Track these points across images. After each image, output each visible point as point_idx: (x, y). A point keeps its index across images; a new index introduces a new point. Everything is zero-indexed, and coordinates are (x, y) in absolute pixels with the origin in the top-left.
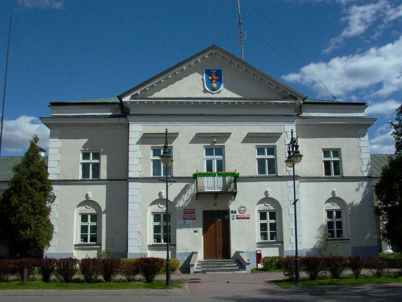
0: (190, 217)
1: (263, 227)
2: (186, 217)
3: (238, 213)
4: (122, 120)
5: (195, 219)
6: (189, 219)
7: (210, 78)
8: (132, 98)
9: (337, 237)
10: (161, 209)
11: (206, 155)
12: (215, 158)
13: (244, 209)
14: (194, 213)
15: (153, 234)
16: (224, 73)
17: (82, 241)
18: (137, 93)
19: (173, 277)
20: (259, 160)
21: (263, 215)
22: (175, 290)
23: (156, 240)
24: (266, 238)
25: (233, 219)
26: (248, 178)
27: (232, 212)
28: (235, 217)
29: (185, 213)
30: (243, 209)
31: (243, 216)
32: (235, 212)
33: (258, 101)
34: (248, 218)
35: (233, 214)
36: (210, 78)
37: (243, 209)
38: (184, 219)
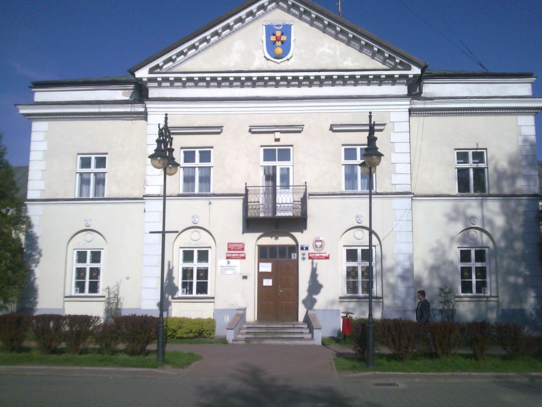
0: (237, 255)
1: (80, 272)
2: (230, 255)
3: (311, 250)
4: (139, 109)
5: (244, 258)
6: (236, 258)
7: (273, 38)
8: (151, 71)
9: (90, 292)
10: (360, 239)
11: (345, 159)
12: (279, 165)
13: (320, 243)
14: (243, 249)
15: (209, 281)
16: (295, 32)
17: (76, 290)
18: (158, 64)
19: (170, 348)
20: (266, 169)
21: (351, 255)
22: (168, 370)
23: (78, 289)
24: (82, 290)
25: (304, 259)
26: (95, 191)
27: (302, 249)
28: (307, 256)
29: (229, 249)
30: (319, 243)
31: (318, 255)
32: (307, 249)
33: (312, 75)
34: (327, 258)
35: (303, 251)
36: (273, 38)
37: (319, 244)
38: (228, 258)
